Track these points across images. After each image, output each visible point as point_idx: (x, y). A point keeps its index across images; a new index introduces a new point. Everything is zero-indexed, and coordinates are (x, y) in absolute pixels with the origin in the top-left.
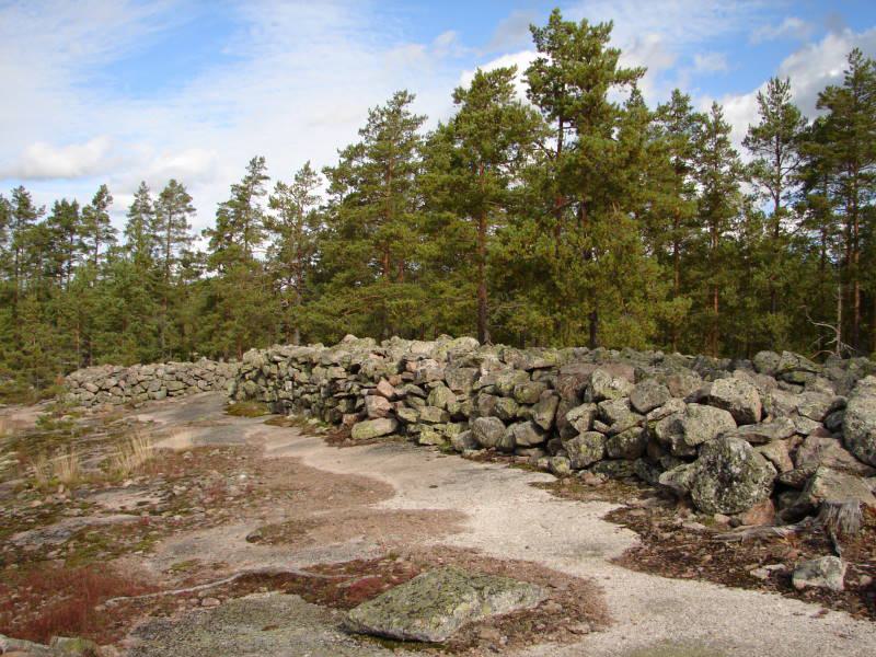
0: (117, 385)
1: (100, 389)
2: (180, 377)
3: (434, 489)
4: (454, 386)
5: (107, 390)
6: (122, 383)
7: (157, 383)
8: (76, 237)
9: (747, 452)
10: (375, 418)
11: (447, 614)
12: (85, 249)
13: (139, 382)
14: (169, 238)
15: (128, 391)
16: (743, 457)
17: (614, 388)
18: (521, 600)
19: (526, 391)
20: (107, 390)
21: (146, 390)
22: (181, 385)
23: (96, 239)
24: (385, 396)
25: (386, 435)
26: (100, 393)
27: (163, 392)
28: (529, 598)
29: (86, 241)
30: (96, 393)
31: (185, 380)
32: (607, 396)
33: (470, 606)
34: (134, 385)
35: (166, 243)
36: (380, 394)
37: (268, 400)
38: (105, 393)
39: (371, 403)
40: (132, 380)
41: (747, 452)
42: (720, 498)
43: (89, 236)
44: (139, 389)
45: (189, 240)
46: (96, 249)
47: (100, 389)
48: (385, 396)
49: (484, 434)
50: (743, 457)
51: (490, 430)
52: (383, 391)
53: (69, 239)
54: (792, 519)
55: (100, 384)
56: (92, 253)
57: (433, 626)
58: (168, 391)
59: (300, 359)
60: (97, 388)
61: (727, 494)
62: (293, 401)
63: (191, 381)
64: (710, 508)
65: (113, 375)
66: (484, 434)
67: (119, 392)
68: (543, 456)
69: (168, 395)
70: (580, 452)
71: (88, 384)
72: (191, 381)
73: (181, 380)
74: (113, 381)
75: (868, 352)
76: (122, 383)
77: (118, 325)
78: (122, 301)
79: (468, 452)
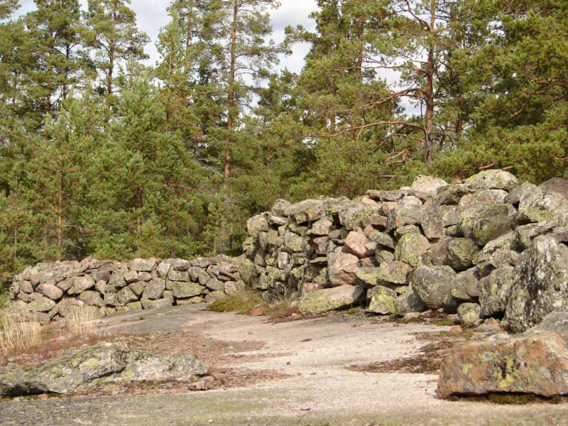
0: (93, 288)
1: (65, 294)
2: (196, 275)
3: (306, 343)
4: (431, 233)
5: (76, 295)
6: (102, 285)
7: (158, 285)
8: (75, 48)
9: (552, 251)
10: (339, 285)
11: (70, 366)
12: (90, 66)
13: (128, 283)
14: (232, 48)
15: (110, 298)
16: (549, 259)
17: (542, 208)
18: (170, 369)
19: (485, 227)
20: (76, 295)
21: (140, 297)
22: (197, 289)
23: (111, 51)
24: (354, 253)
25: (345, 307)
26: (64, 301)
27: (168, 300)
28: (180, 368)
29: (93, 54)
30: (57, 301)
31: (203, 281)
32: (532, 219)
33: (102, 363)
34: (119, 288)
35: (228, 56)
36: (348, 250)
37: (263, 287)
38: (73, 299)
39: (334, 262)
40: (118, 279)
41: (552, 251)
42: (528, 314)
43: (99, 45)
44: (127, 294)
45: (270, 53)
46: (111, 68)
47: (65, 294)
48: (354, 253)
49: (425, 288)
50: (549, 259)
51: (433, 282)
52: (352, 246)
53: (64, 51)
54: (541, 319)
55: (64, 285)
56: (102, 75)
57: (53, 376)
58: (175, 298)
59: (298, 217)
60: (60, 293)
61: (534, 306)
62: (286, 282)
63: (214, 283)
64: (518, 326)
65: (87, 272)
66: (425, 288)
67: (95, 298)
68: (501, 320)
69: (175, 304)
70: (490, 294)
71: (46, 286)
72: (214, 283)
73: (197, 281)
74: (87, 282)
75: (7, 28)
76: (102, 285)
77: (131, 199)
78: (138, 156)
79: (409, 315)
